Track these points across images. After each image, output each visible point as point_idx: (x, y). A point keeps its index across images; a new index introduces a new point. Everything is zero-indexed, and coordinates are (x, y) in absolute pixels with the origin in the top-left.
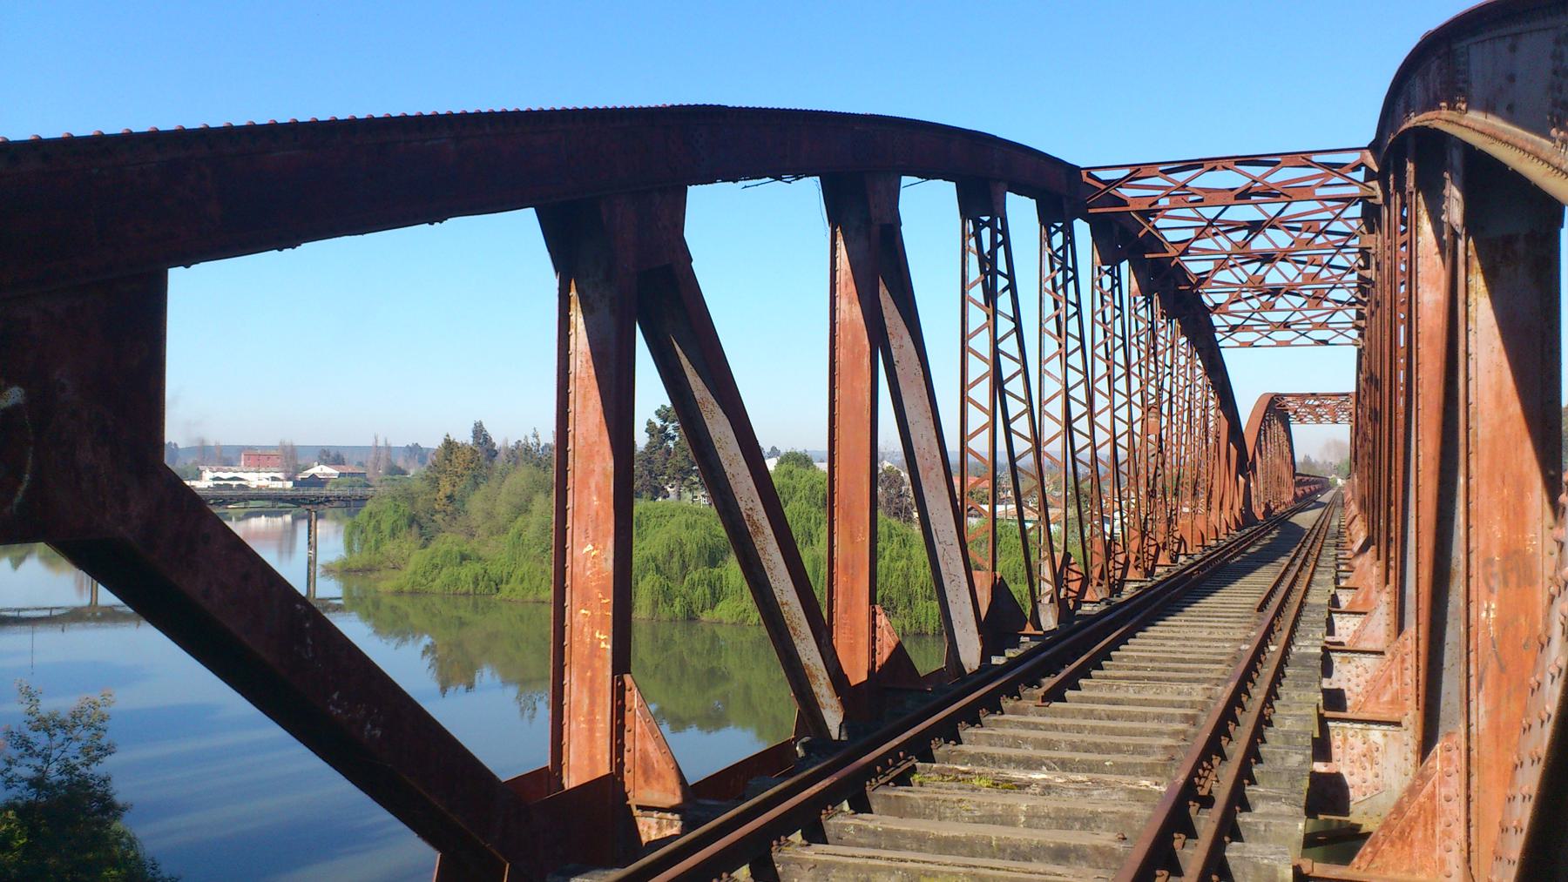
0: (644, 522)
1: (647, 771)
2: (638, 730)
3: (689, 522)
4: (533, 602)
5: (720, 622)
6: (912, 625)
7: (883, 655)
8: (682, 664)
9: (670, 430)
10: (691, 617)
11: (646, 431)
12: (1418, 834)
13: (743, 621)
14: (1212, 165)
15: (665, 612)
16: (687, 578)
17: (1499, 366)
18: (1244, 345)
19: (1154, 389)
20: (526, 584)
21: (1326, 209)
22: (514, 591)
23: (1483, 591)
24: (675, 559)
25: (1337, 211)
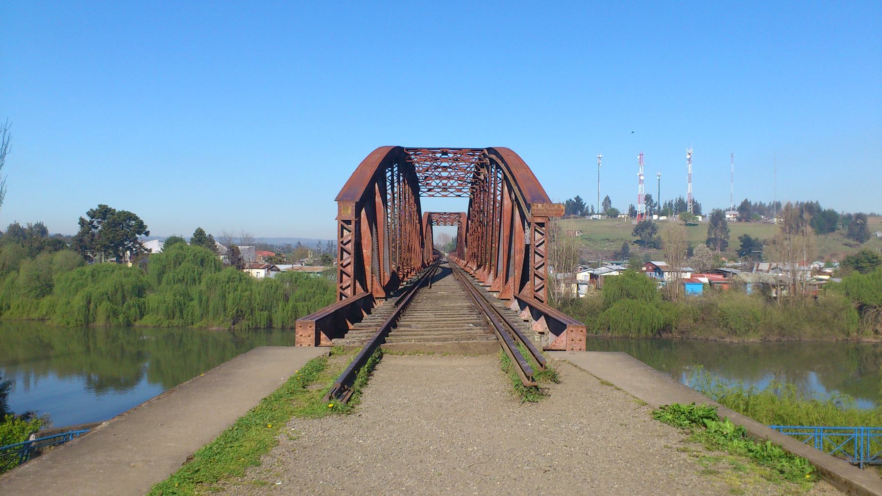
0: (97, 274)
3: (126, 273)
5: (146, 327)
6: (252, 324)
7: (387, 279)
8: (123, 351)
10: (129, 325)
11: (79, 224)
15: (114, 322)
16: (125, 304)
20: (21, 309)
22: (13, 314)
24: (119, 293)
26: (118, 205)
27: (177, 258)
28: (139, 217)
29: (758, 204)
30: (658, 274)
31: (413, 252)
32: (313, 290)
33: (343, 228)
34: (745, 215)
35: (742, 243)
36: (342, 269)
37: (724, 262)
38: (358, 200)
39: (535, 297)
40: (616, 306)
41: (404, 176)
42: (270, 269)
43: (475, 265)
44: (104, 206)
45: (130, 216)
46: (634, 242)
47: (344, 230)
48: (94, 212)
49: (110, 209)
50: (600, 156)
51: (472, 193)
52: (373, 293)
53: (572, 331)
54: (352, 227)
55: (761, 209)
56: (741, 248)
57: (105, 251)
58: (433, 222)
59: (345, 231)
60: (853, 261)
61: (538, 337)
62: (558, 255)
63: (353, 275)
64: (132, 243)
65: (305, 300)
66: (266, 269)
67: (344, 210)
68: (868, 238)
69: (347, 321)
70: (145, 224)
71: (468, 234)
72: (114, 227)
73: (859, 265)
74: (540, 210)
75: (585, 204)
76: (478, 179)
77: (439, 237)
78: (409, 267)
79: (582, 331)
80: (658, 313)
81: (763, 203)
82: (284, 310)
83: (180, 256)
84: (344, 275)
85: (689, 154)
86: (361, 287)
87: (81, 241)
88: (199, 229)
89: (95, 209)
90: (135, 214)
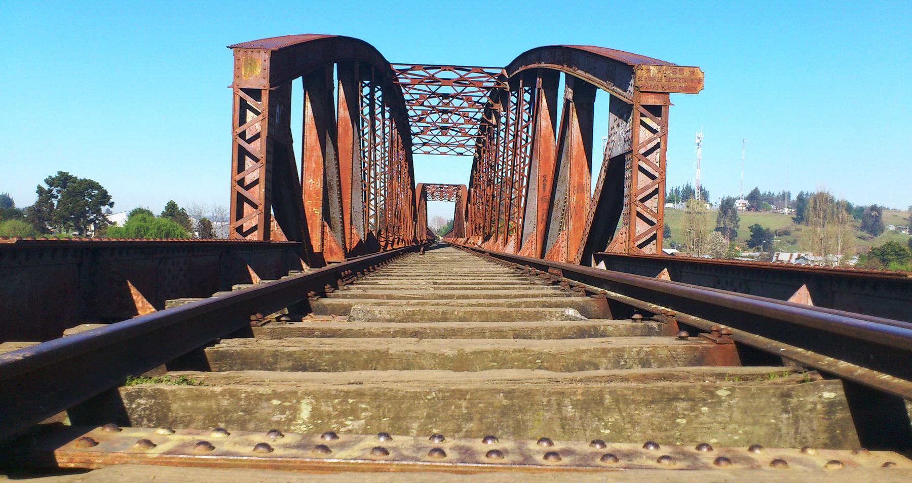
1: (332, 252)
2: (328, 239)
9: (54, 192)
11: (37, 192)
14: (445, 68)
17: (579, 136)
18: (425, 153)
19: (501, 135)
21: (480, 91)
23: (573, 194)
25: (485, 92)
26: (80, 173)
27: (139, 231)
28: (102, 186)
29: (767, 193)
31: (402, 220)
33: (243, 102)
34: (755, 204)
35: (752, 233)
36: (242, 191)
37: (738, 252)
41: (390, 112)
43: (481, 238)
44: (64, 173)
45: (92, 185)
47: (248, 111)
48: (53, 179)
49: (71, 177)
51: (478, 151)
52: (325, 254)
54: (263, 105)
55: (770, 199)
56: (751, 238)
57: (64, 223)
60: (879, 253)
63: (263, 204)
64: (95, 215)
67: (246, 67)
68: (882, 231)
69: (133, 290)
70: (109, 194)
72: (74, 196)
73: (885, 257)
74: (653, 79)
76: (489, 123)
77: (434, 220)
78: (396, 237)
81: (772, 193)
83: (142, 229)
84: (246, 205)
85: (699, 138)
86: (280, 229)
87: (39, 211)
88: (171, 202)
89: (54, 177)
90: (98, 183)
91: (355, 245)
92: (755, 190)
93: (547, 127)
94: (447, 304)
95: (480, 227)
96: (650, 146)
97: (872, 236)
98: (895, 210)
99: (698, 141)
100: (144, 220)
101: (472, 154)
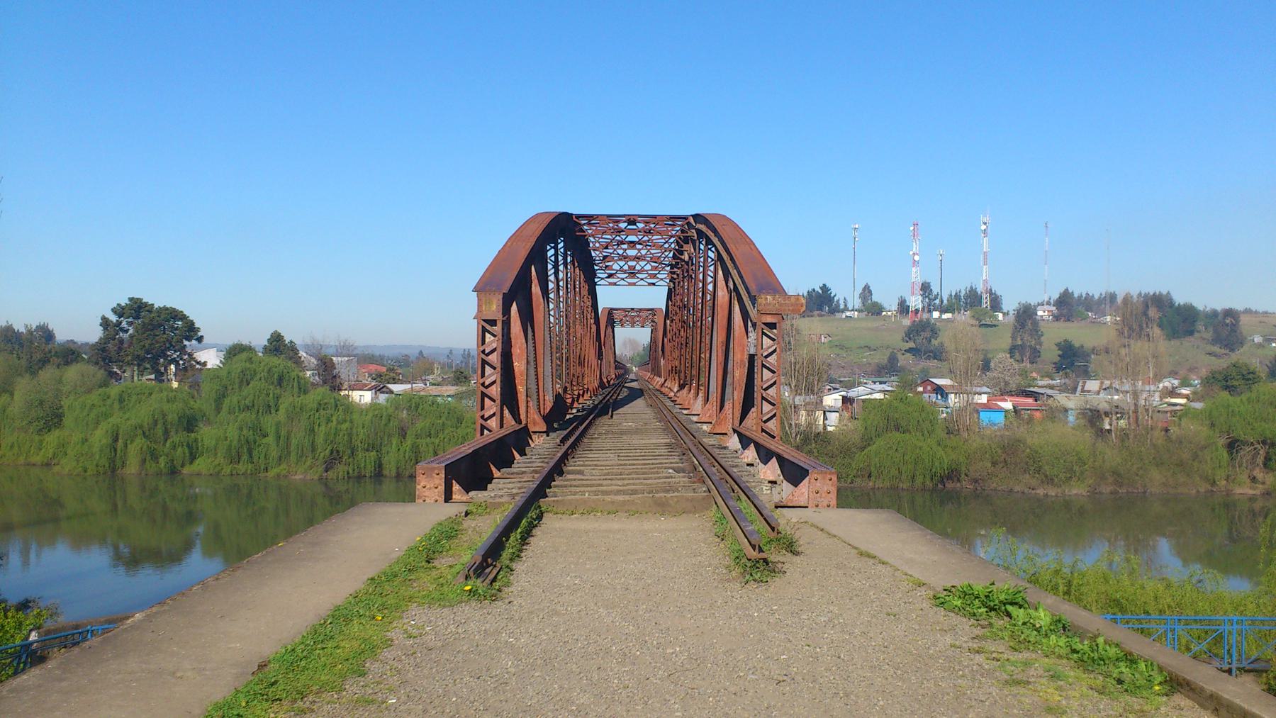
1: (535, 424)
4: (24, 465)
5: (199, 474)
8: (165, 508)
10: (173, 472)
11: (101, 325)
12: (723, 423)
13: (219, 472)
15: (151, 467)
20: (16, 450)
24: (159, 426)
26: (158, 298)
29: (1084, 296)
30: (939, 397)
31: (586, 365)
32: (441, 421)
35: (1060, 353)
37: (1035, 379)
38: (506, 291)
39: (763, 430)
40: (880, 443)
42: (379, 390)
44: (138, 299)
45: (175, 315)
46: (905, 351)
47: (486, 333)
48: (123, 308)
49: (146, 304)
50: (857, 226)
51: (672, 280)
53: (816, 480)
54: (497, 329)
55: (1088, 303)
56: (1059, 358)
58: (614, 322)
59: (488, 335)
60: (1220, 378)
61: (767, 488)
62: (797, 369)
64: (178, 353)
65: (430, 436)
66: (374, 391)
67: (486, 305)
68: (1242, 344)
69: (492, 466)
70: (196, 326)
71: (666, 340)
72: (152, 330)
75: (835, 296)
76: (681, 259)
77: (624, 344)
79: (830, 480)
80: (940, 452)
81: (1091, 294)
82: (399, 450)
84: (486, 399)
85: (985, 224)
86: (510, 416)
87: (104, 350)
88: (276, 332)
89: (123, 304)
91: (548, 410)
92: (1064, 292)
93: (723, 296)
94: (622, 469)
95: (672, 370)
96: (770, 350)
97: (1227, 352)
98: (1266, 313)
99: (983, 227)
100: (250, 360)
101: (666, 284)
